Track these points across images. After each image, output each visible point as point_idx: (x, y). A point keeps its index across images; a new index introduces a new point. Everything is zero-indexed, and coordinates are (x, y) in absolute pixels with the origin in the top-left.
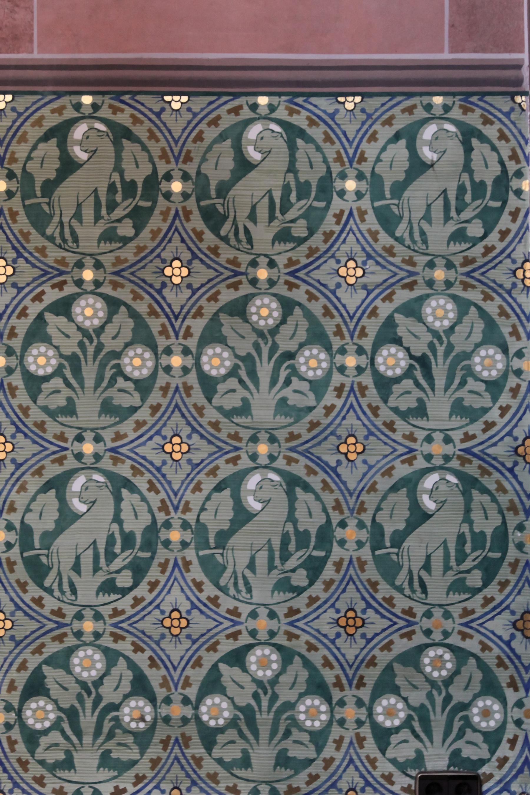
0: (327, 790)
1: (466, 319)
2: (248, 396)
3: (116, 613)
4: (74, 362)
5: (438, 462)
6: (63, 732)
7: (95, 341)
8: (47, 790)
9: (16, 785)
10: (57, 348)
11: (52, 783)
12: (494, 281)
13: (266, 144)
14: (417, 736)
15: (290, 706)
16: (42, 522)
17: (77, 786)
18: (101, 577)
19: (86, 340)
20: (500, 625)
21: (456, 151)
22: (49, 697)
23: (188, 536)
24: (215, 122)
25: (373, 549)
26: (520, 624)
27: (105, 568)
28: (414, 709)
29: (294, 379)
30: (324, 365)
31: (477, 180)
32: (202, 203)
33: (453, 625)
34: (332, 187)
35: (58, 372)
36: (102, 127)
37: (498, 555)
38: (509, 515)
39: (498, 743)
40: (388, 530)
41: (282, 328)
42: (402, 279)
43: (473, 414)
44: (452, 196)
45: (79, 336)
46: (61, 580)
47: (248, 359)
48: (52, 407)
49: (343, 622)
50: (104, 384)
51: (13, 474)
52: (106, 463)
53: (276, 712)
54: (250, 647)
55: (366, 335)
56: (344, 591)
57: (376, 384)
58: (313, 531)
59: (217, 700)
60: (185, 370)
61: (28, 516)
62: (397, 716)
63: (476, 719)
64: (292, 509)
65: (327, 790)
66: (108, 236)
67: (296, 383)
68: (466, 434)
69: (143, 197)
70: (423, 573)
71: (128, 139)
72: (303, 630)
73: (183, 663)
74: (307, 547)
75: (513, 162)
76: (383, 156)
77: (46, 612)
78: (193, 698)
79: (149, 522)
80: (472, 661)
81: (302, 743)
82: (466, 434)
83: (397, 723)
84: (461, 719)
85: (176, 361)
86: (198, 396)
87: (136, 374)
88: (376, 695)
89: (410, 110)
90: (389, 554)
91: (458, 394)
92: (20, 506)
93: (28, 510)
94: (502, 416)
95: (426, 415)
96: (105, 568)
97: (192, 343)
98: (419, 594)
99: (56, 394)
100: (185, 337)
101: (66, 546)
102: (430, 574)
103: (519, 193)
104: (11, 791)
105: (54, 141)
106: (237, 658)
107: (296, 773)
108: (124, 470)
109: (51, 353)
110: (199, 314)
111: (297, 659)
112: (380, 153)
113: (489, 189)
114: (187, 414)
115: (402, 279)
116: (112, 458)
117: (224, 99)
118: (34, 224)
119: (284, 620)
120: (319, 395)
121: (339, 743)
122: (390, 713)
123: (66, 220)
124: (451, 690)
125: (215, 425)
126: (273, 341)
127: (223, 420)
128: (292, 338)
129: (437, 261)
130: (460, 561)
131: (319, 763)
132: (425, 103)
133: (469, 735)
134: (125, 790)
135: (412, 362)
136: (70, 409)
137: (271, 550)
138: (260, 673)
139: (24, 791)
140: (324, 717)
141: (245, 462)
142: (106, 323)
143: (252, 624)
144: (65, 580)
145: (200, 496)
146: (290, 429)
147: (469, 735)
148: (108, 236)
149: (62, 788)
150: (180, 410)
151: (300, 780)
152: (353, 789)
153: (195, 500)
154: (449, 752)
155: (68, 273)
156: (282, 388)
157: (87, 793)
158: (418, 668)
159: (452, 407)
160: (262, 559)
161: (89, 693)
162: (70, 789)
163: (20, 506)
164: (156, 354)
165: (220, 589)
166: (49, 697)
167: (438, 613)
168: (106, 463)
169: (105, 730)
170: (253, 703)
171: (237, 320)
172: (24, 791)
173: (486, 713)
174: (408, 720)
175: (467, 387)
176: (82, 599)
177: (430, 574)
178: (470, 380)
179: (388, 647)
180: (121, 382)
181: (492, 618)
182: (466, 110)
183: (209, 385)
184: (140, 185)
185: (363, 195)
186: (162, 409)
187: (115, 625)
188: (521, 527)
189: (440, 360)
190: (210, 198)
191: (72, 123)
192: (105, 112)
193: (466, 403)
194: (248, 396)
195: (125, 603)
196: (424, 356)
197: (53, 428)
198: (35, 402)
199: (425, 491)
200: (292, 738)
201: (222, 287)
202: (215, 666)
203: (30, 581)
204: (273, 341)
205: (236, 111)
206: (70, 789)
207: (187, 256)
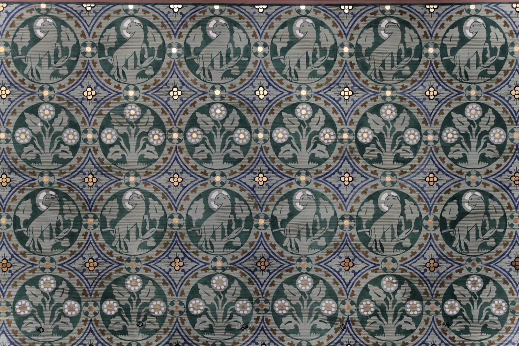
0: (250, 344)
1: (486, 114)
2: (124, 153)
3: (403, 259)
4: (381, 136)
5: (389, 185)
6: (208, 316)
7: (391, 127)
8: (285, 343)
9: (271, 341)
10: (373, 130)
11: (288, 340)
12: (245, 97)
13: (305, 30)
14: (380, 320)
15: (60, 305)
16: (24, 216)
17: (128, 342)
18: (479, 242)
19: (387, 126)
20: (505, 264)
21: (483, 33)
22: (201, 298)
23: (182, 222)
24: (450, 18)
25: (15, 228)
26: (514, 264)
27: (397, 238)
28: (208, 305)
29: (147, 145)
30: (333, 138)
31: (236, 47)
32: (444, 58)
33: (312, 265)
34: (508, 50)
35: (32, 142)
36: (395, 21)
37: (502, 230)
38: (507, 211)
39: (77, 322)
40: (194, 219)
41: (482, 119)
42: (371, 96)
43: (235, 162)
44: (310, 55)
45: (468, 124)
46: (460, 243)
47: (296, 135)
48: (115, 159)
49: (343, 264)
50: (140, 148)
51: (181, 192)
52: (227, 186)
53: (226, 306)
54: (468, 276)
55: (182, 123)
56: (513, 248)
57: (15, 147)
58: (158, 219)
59: (198, 301)
60: (94, 141)
61: (104, 212)
62: (246, 309)
63: (238, 309)
64: (403, 209)
65: (250, 344)
66: (55, 74)
67: (148, 147)
68: (402, 171)
69: (158, 56)
70: (212, 240)
71: (494, 26)
72: (408, 268)
73: (180, 284)
74: (495, 227)
75: (83, 38)
76: (447, 35)
77: (285, 258)
78: (356, 301)
79: (248, 215)
80: (150, 282)
81: (324, 322)
82: (402, 171)
83: (455, 313)
84: (59, 311)
85: (90, 136)
86: (271, 153)
87: (411, 143)
88: (445, 300)
89: (460, 12)
90: (195, 230)
91: (483, 151)
92: (186, 207)
93: (190, 209)
94: (419, 162)
95: (40, 162)
96: (397, 238)
97: (269, 127)
98: (210, 250)
99: (201, 153)
100: (350, 125)
101: (123, 226)
102: (300, 240)
103: (512, 54)
104: (269, 344)
105: (457, 28)
106: (207, 281)
107: (492, 336)
108: (150, 189)
109: (455, 132)
110: (14, 113)
111: (236, 281)
112: (103, 33)
113: (499, 51)
114: (436, 162)
115: (114, 96)
116: (229, 183)
117: (286, 7)
118: (18, 68)
119: (399, 263)
120: (415, 152)
121: (426, 321)
122: (452, 307)
123: (292, 68)
124: (54, 297)
125: (195, 168)
126: (478, 126)
127: (284, 165)
128: (487, 124)
129: (130, 87)
130: (143, 233)
131: (417, 331)
132: (211, 8)
133: (63, 319)
134: (151, 344)
135: (290, 136)
136: (209, 159)
137: (393, 229)
138: (473, 289)
139: (103, 344)
140: (163, 309)
141: (123, 186)
142: (482, 117)
143: (298, 265)
144: (462, 244)
145: (188, 203)
146: (487, 168)
147: (406, 318)
148: (55, 74)
149: (377, 342)
150: (263, 160)
151: (324, 339)
152: (264, 344)
153: (186, 204)
154: (311, 326)
155: (378, 93)
156: (397, 149)
157: (304, 344)
158: (124, 286)
159: (225, 157)
160: (473, 233)
161: (476, 298)
162: (296, 342)
163: (186, 207)
164: (251, 132)
165: (112, 247)
166: (201, 298)
167: (474, 259)
168: (227, 186)
169: (484, 315)
170: (215, 303)
171: (33, 116)
172: (275, 344)
173: (452, 307)
174: (291, 310)
175: (317, 148)
176: (216, 251)
177: (300, 240)
178: (62, 145)
179: (365, 277)
180: (148, 147)
181: (415, 262)
182: (316, 12)
183: (277, 147)
184: (156, 50)
185: (95, 54)
186: (254, 159)
187: (402, 265)
188: (512, 217)
189: (389, 135)
190: (447, 56)
191: (466, 19)
192: (312, 14)
193: (60, 157)
194: (380, 152)
195: (407, 255)
196: (125, 133)
197: (286, 168)
198: (277, 156)
199: (297, 201)
200: (318, 319)
201: (197, 99)
202: (281, 285)
203: (19, 244)
204: (478, 126)
205: (460, 12)
206: (296, 342)
207: (351, 85)
